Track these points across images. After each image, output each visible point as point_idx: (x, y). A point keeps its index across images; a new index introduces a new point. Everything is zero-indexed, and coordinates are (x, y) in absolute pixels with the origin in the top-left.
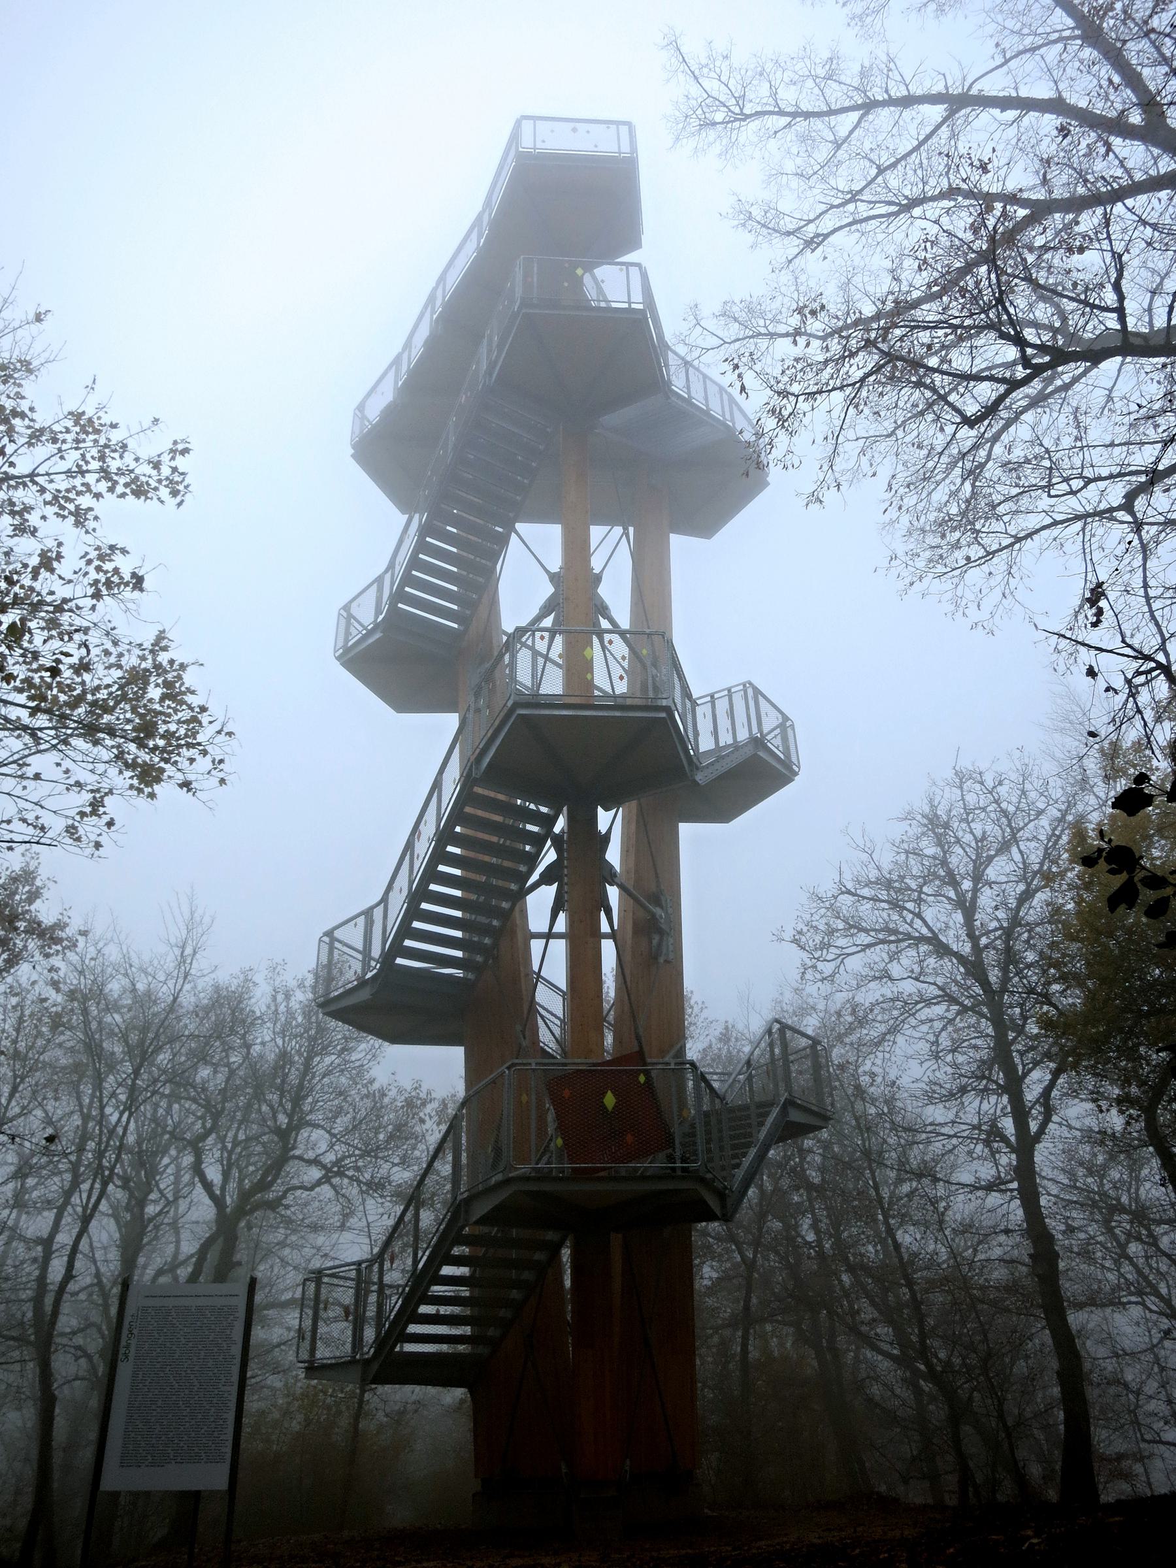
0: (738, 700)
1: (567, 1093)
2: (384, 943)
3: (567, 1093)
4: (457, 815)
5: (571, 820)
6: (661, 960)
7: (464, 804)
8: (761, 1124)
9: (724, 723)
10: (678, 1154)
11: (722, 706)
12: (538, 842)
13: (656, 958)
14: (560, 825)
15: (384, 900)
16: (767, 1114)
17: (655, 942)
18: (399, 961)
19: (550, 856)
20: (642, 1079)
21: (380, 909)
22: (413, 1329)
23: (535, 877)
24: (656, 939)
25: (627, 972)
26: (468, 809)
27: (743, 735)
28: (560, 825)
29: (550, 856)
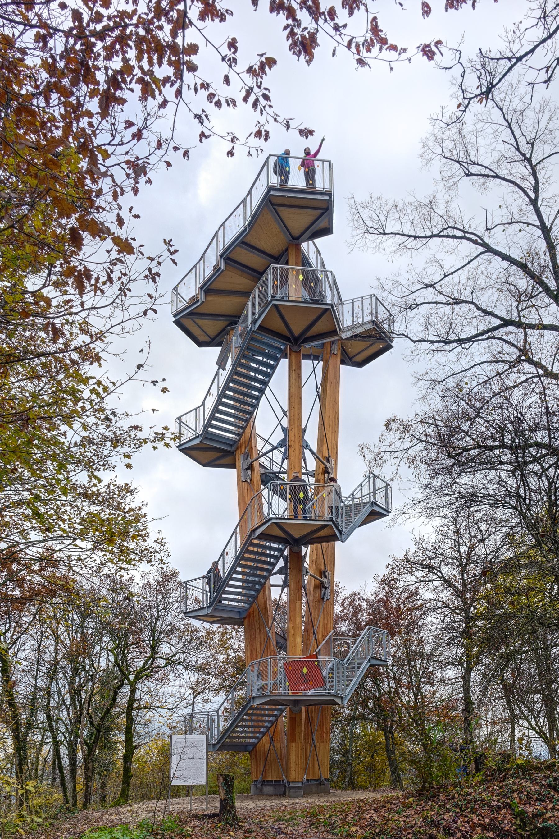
0: (367, 302)
1: (290, 668)
2: (204, 421)
3: (290, 668)
4: (226, 387)
5: (291, 551)
6: (325, 600)
7: (230, 382)
8: (359, 668)
9: (357, 310)
10: (327, 688)
11: (357, 304)
12: (277, 558)
13: (323, 599)
14: (286, 553)
15: (203, 404)
16: (362, 663)
17: (323, 592)
18: (210, 429)
19: (281, 563)
20: (316, 663)
21: (202, 408)
22: (231, 582)
23: (275, 571)
24: (323, 590)
25: (311, 604)
26: (231, 385)
27: (367, 318)
28: (286, 553)
29: (281, 563)
